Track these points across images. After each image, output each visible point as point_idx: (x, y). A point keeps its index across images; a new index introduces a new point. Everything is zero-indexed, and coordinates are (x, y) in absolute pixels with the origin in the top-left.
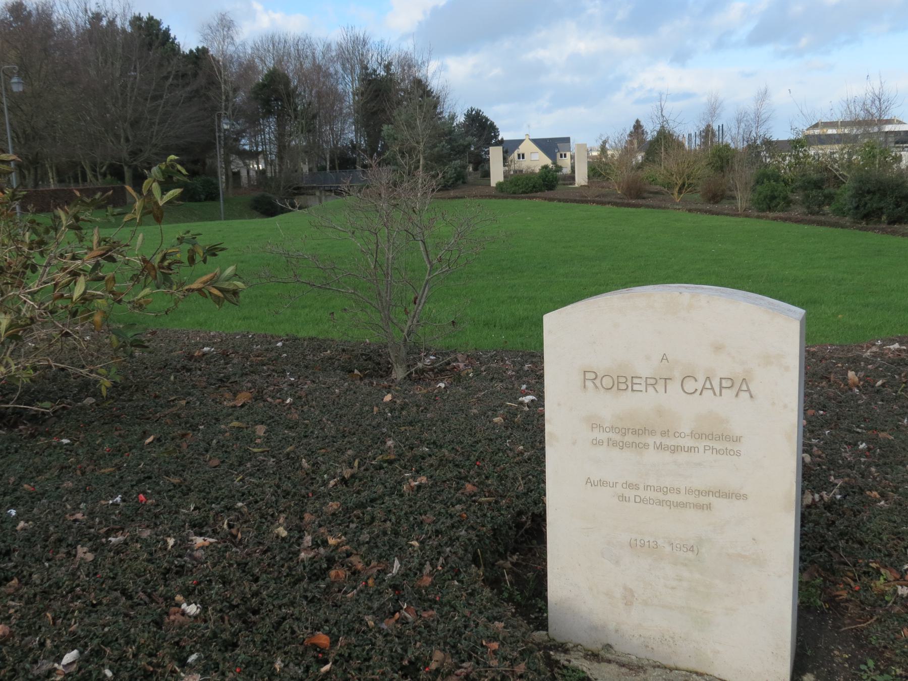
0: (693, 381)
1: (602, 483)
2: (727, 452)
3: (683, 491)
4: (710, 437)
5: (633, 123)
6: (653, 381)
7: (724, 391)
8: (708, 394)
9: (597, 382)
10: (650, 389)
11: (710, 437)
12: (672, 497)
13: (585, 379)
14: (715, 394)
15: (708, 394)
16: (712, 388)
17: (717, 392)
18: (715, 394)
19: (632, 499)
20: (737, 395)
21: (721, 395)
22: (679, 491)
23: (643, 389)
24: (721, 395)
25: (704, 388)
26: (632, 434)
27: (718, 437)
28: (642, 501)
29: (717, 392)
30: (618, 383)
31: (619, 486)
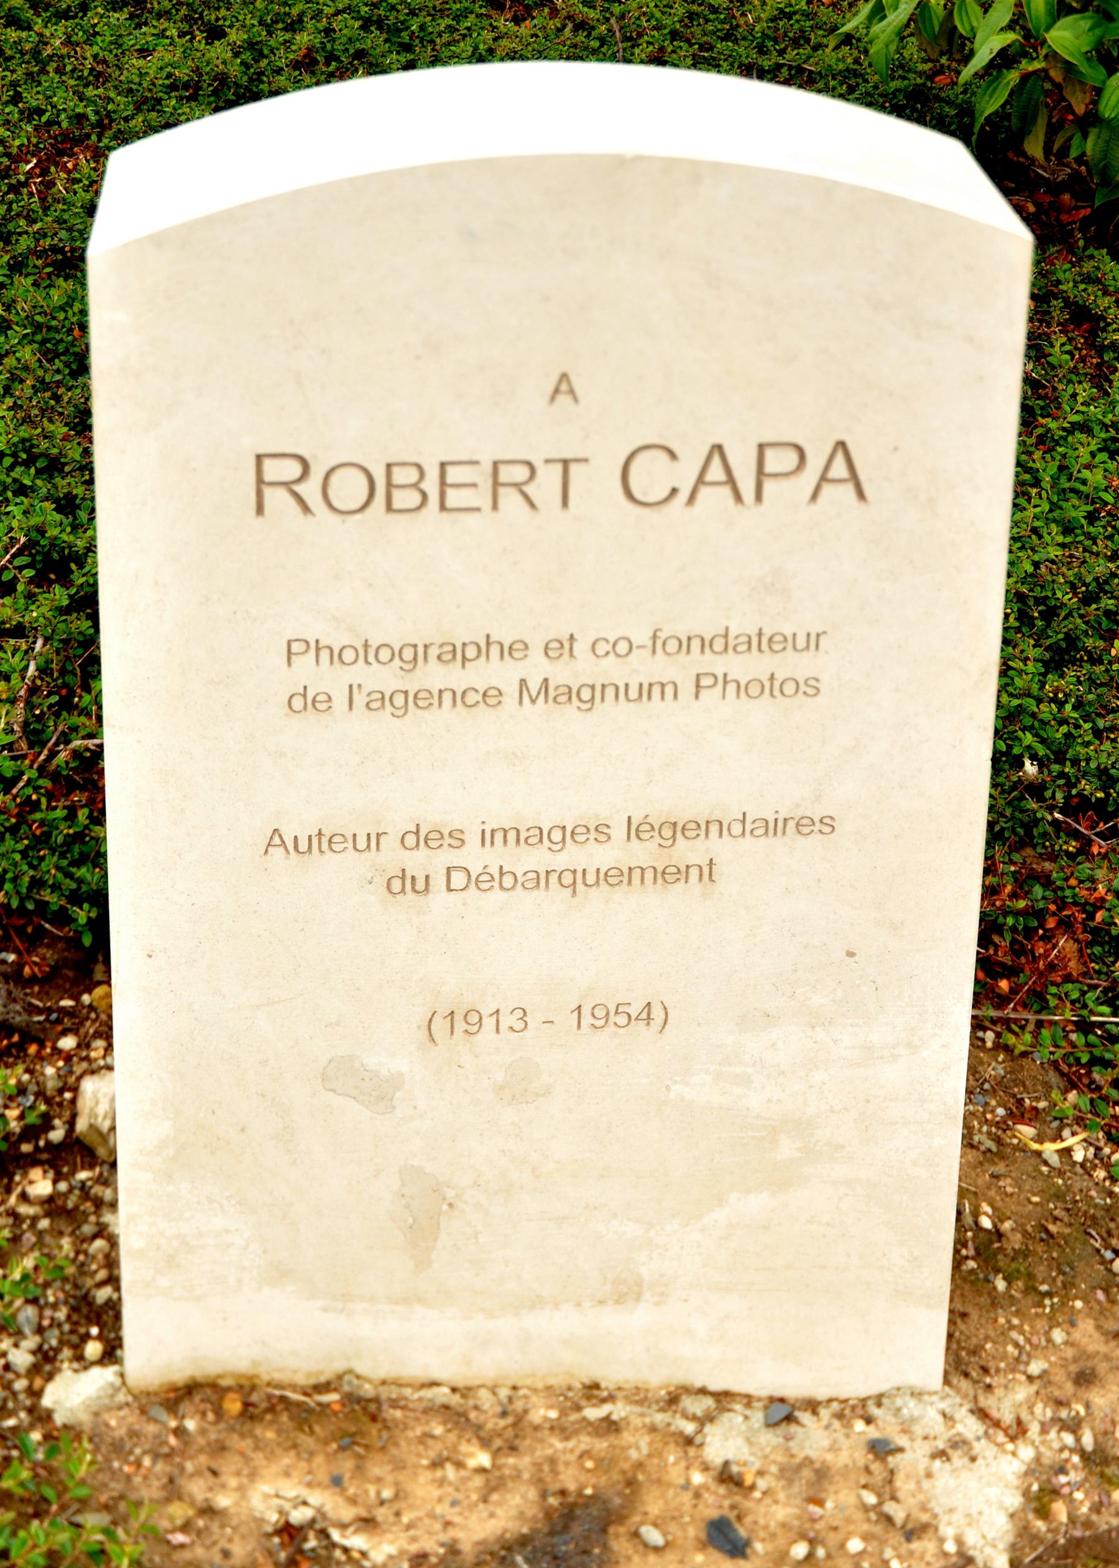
0: (664, 457)
1: (322, 841)
2: (772, 686)
3: (618, 832)
4: (719, 645)
5: (1115, 15)
6: (520, 473)
7: (769, 486)
8: (715, 498)
9: (310, 490)
10: (510, 499)
11: (719, 645)
12: (573, 857)
13: (260, 481)
14: (738, 497)
15: (715, 498)
16: (731, 481)
17: (747, 487)
18: (738, 497)
19: (438, 882)
20: (815, 496)
21: (759, 497)
22: (602, 832)
23: (486, 503)
24: (759, 497)
25: (700, 480)
26: (282, 480)
27: (758, 661)
28: (474, 881)
29: (747, 487)
30: (389, 485)
31: (390, 843)
